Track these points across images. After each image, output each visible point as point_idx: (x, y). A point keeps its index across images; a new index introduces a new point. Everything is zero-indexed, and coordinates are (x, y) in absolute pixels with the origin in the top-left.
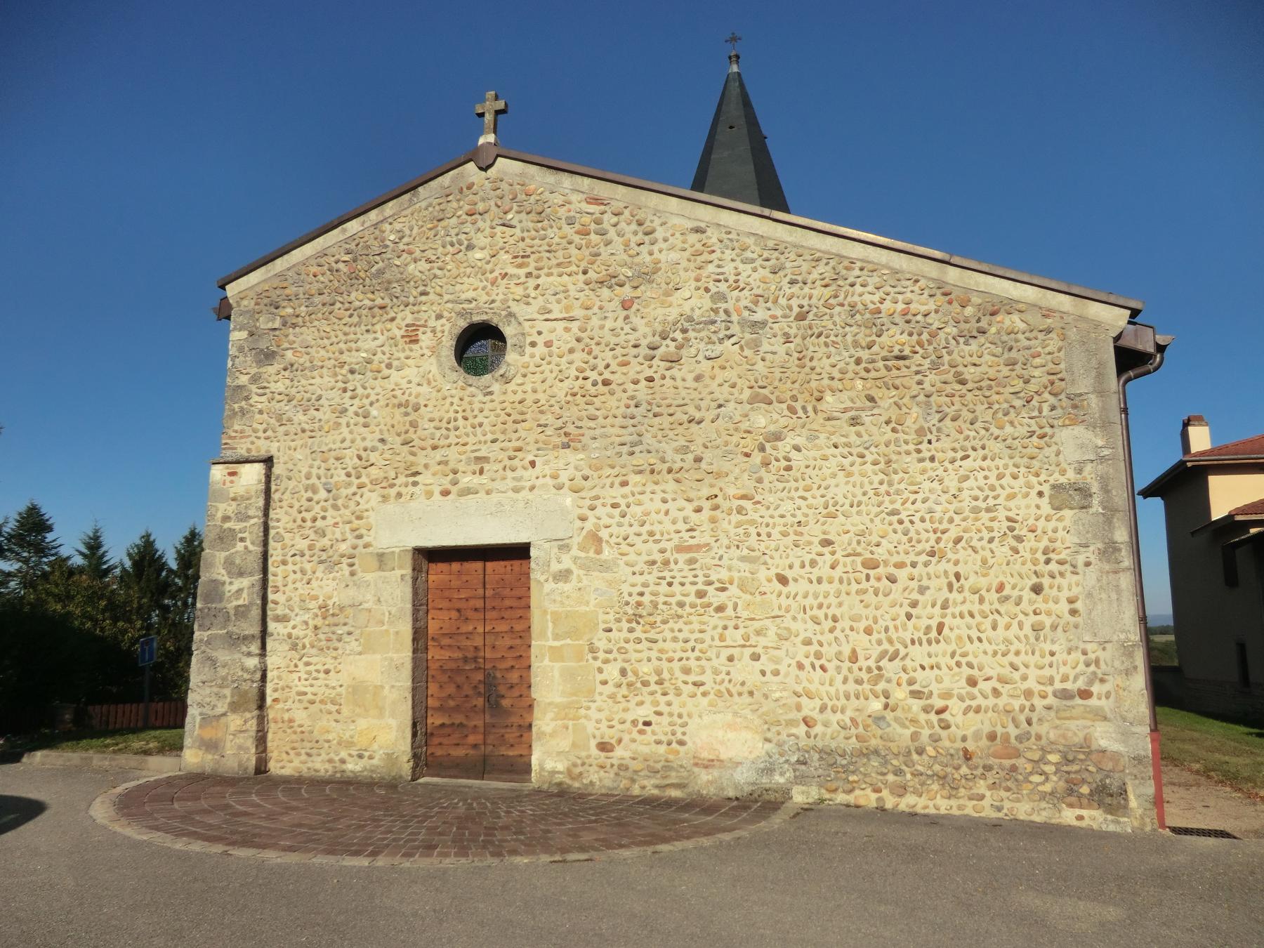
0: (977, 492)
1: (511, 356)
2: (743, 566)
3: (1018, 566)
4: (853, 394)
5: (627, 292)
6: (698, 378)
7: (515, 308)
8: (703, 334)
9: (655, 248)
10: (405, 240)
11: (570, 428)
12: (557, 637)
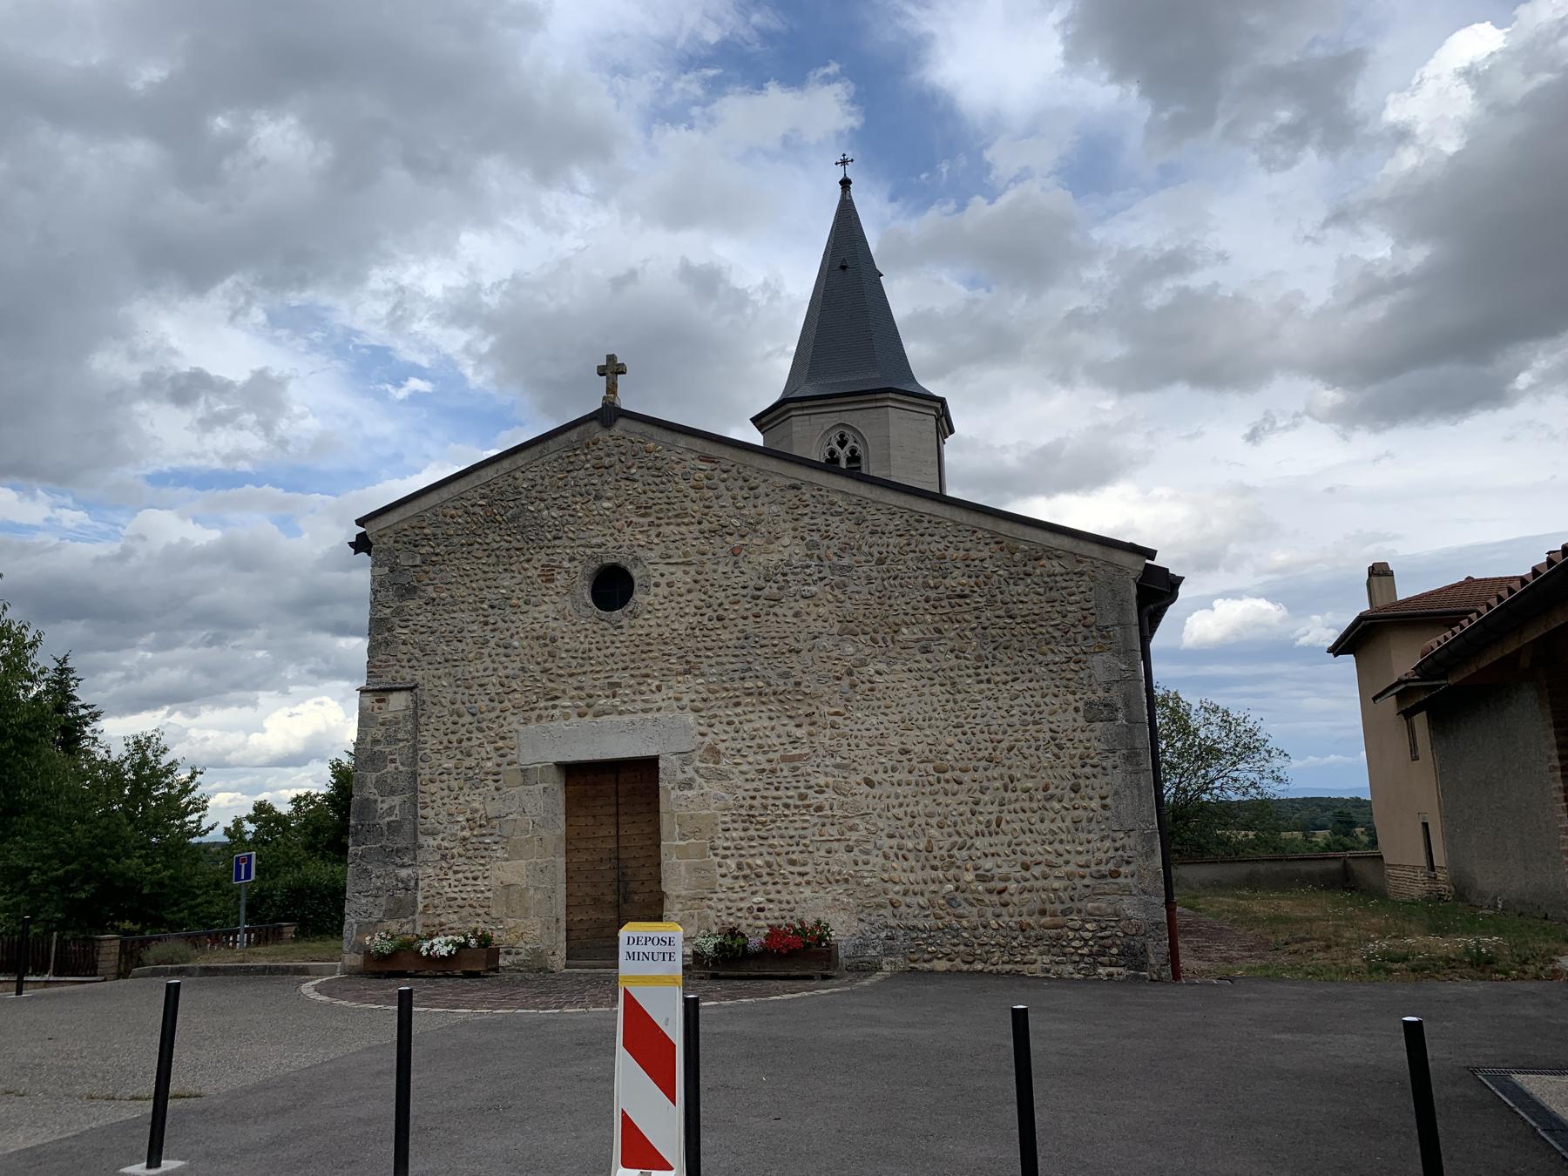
0: (1026, 709)
1: (638, 596)
2: (836, 772)
3: (1059, 770)
4: (923, 627)
5: (735, 541)
6: (796, 615)
7: (640, 553)
8: (799, 577)
9: (759, 502)
10: (538, 488)
11: (691, 658)
12: (683, 837)
